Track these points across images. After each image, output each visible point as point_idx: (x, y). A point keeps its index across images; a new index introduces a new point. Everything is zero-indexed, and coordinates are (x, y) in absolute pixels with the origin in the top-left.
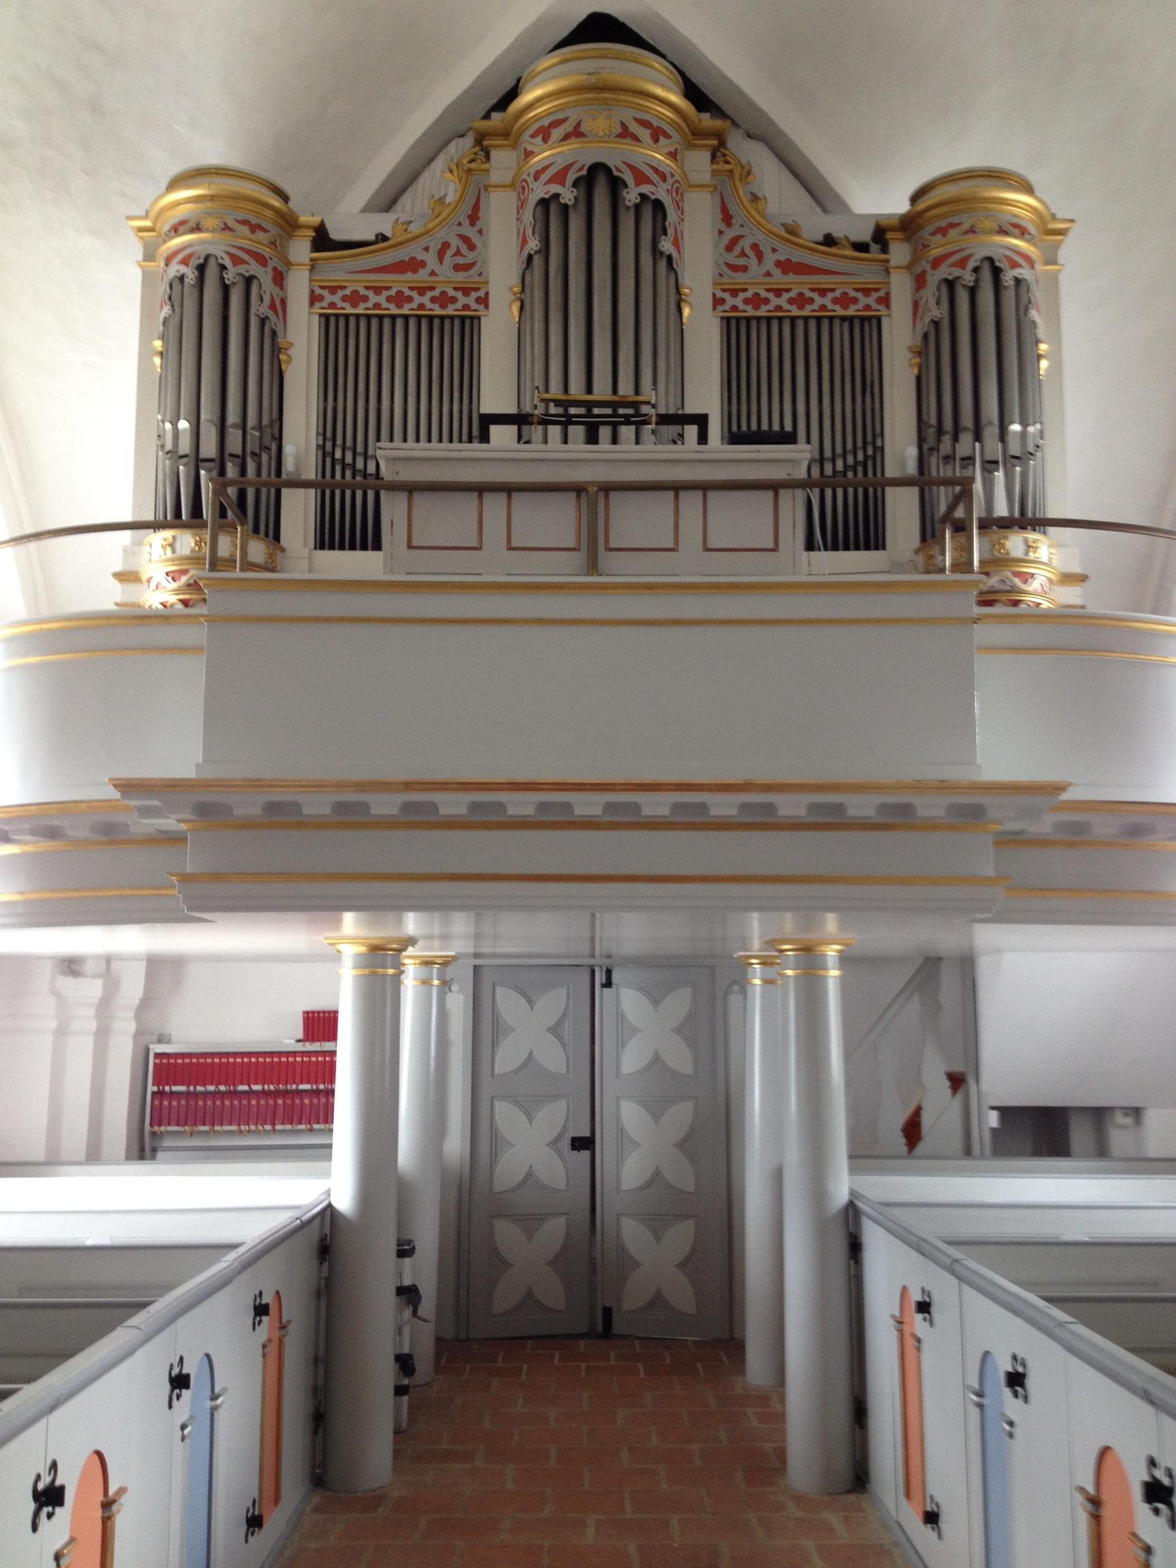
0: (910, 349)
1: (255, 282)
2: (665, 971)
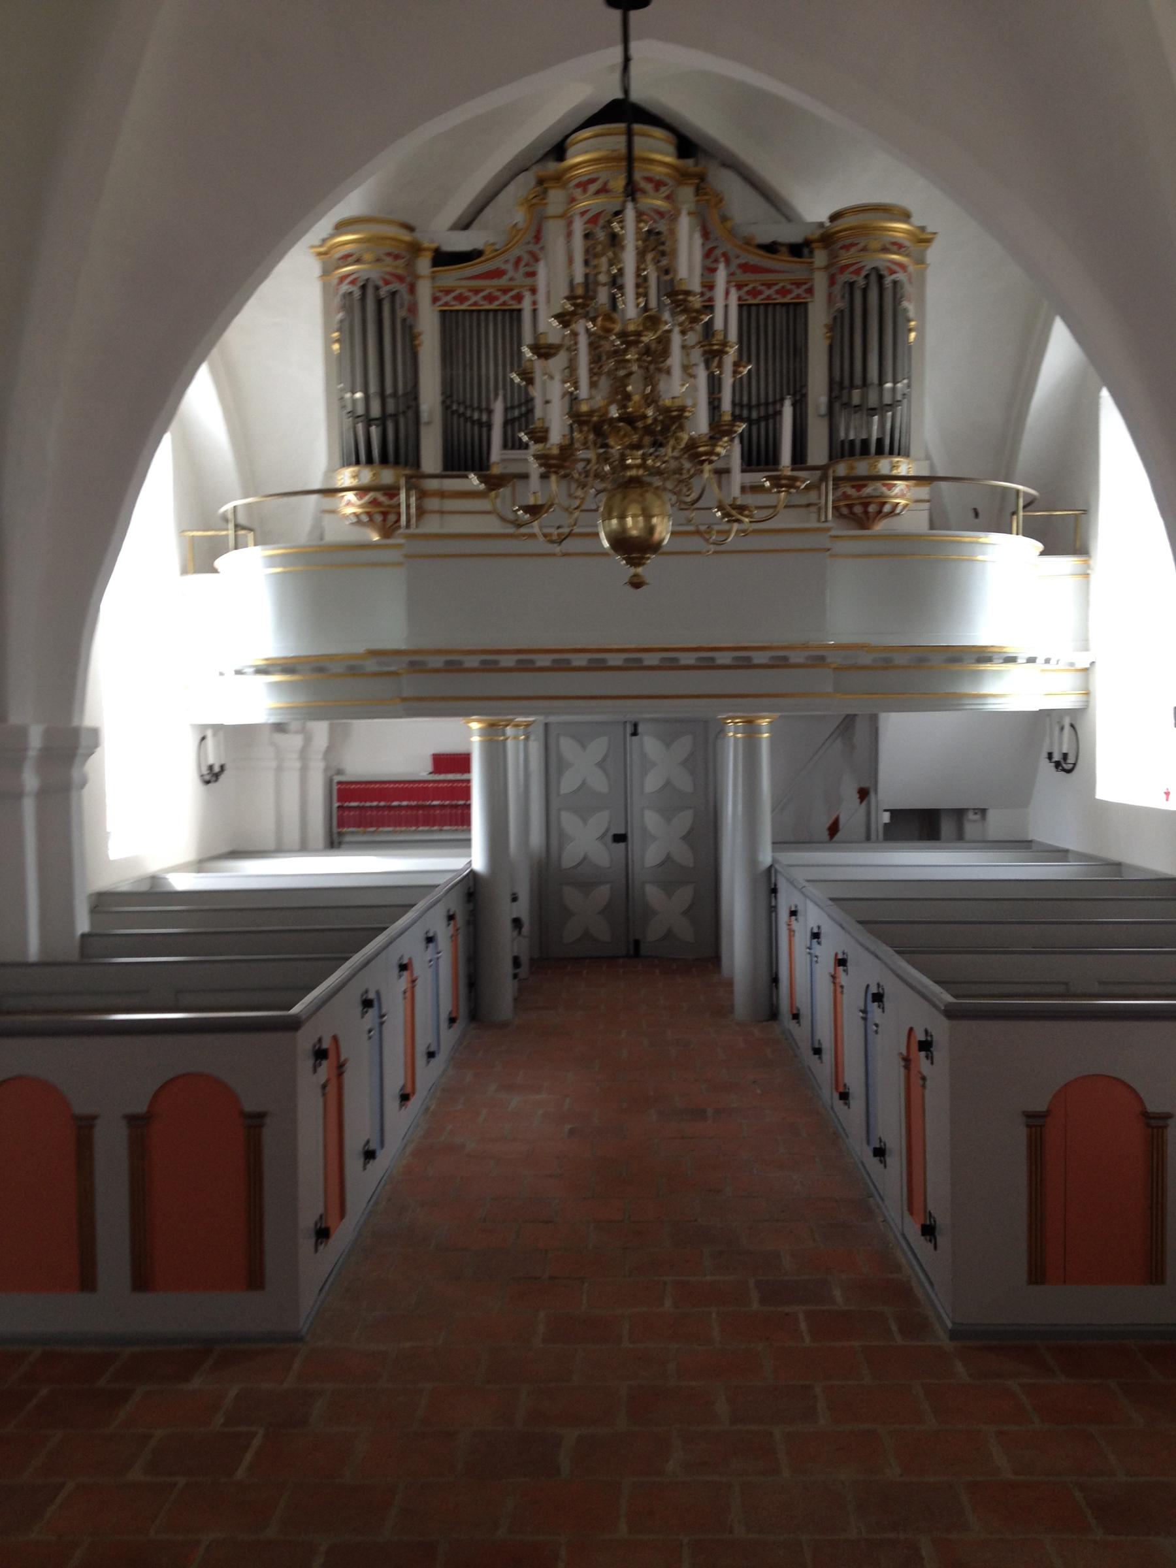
0: (826, 326)
1: (398, 296)
2: (671, 730)
